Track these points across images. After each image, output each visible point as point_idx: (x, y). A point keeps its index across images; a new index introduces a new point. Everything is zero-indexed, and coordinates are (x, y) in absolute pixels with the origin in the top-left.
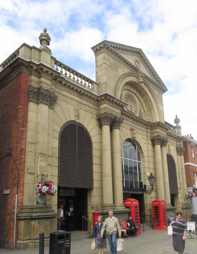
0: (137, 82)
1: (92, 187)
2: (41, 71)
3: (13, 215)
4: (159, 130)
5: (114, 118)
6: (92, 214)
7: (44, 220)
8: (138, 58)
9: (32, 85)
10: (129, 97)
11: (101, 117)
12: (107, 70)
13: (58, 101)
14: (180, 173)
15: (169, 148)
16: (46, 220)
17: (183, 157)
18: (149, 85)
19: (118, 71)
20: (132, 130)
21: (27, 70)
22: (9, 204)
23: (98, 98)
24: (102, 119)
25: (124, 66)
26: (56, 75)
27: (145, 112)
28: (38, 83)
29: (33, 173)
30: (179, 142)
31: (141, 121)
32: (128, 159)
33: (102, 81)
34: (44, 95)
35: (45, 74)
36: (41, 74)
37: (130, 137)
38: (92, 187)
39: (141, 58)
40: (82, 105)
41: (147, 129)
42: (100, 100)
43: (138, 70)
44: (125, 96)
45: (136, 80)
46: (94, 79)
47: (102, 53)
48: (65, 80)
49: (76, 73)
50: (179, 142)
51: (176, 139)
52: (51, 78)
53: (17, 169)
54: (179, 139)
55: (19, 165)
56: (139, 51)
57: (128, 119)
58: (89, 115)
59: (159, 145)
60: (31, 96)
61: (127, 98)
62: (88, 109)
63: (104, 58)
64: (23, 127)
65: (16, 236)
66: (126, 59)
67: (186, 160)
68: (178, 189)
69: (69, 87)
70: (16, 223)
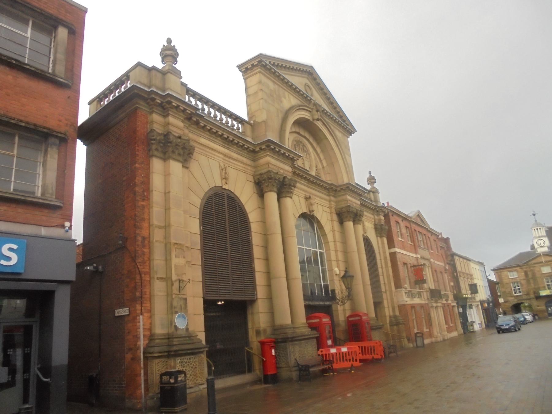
0: (311, 120)
1: (256, 298)
2: (168, 106)
3: (138, 351)
4: (349, 197)
5: (283, 180)
6: (259, 344)
7: (188, 357)
8: (308, 80)
9: (154, 128)
10: (299, 145)
11: (262, 179)
12: (266, 101)
13: (195, 154)
14: (384, 266)
15: (364, 226)
16: (192, 358)
17: (385, 240)
18: (330, 125)
19: (281, 102)
20: (307, 198)
21: (146, 105)
22: (129, 333)
23: (256, 147)
24: (263, 182)
25: (290, 95)
26: (192, 111)
27: (323, 167)
28: (58, 77)
29: (164, 278)
30: (378, 215)
31: (320, 183)
32: (304, 247)
33: (259, 120)
34: (174, 145)
35: (174, 110)
36: (168, 110)
37: (305, 210)
38: (254, 297)
39: (313, 81)
40: (231, 161)
41: (329, 196)
42: (259, 151)
43: (312, 101)
44: (292, 144)
45: (309, 116)
46: (245, 116)
47: (256, 74)
48: (204, 120)
49: (240, 120)
50: (378, 215)
51: (372, 211)
52: (184, 116)
53: (137, 272)
54: (377, 210)
55: (141, 266)
56: (309, 71)
57: (300, 181)
58: (242, 176)
59: (351, 221)
60: (154, 147)
61: (296, 146)
62: (239, 166)
63: (260, 82)
64: (143, 200)
65: (145, 388)
66: (293, 83)
67: (391, 244)
68: (383, 293)
69: (210, 130)
70: (144, 364)
